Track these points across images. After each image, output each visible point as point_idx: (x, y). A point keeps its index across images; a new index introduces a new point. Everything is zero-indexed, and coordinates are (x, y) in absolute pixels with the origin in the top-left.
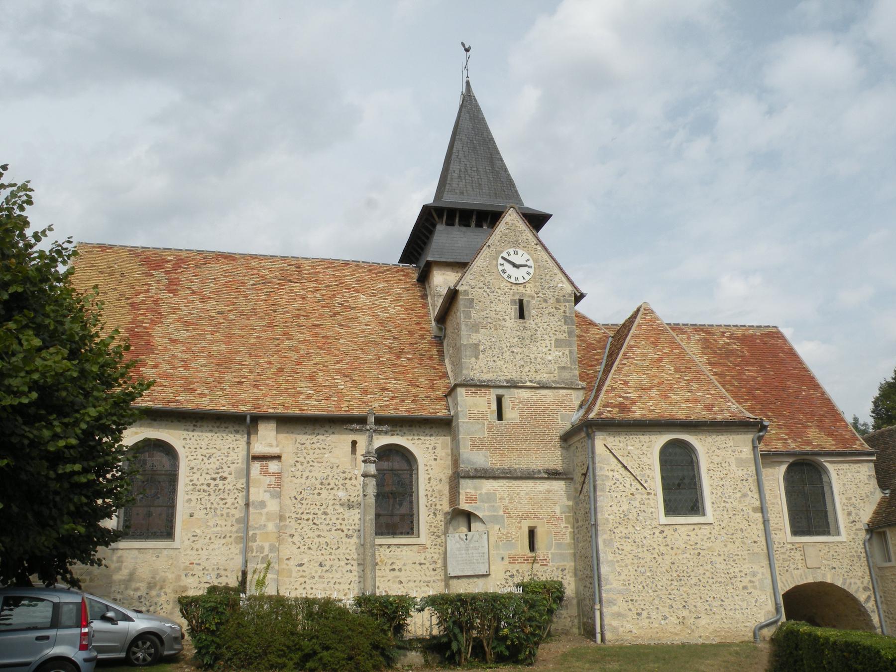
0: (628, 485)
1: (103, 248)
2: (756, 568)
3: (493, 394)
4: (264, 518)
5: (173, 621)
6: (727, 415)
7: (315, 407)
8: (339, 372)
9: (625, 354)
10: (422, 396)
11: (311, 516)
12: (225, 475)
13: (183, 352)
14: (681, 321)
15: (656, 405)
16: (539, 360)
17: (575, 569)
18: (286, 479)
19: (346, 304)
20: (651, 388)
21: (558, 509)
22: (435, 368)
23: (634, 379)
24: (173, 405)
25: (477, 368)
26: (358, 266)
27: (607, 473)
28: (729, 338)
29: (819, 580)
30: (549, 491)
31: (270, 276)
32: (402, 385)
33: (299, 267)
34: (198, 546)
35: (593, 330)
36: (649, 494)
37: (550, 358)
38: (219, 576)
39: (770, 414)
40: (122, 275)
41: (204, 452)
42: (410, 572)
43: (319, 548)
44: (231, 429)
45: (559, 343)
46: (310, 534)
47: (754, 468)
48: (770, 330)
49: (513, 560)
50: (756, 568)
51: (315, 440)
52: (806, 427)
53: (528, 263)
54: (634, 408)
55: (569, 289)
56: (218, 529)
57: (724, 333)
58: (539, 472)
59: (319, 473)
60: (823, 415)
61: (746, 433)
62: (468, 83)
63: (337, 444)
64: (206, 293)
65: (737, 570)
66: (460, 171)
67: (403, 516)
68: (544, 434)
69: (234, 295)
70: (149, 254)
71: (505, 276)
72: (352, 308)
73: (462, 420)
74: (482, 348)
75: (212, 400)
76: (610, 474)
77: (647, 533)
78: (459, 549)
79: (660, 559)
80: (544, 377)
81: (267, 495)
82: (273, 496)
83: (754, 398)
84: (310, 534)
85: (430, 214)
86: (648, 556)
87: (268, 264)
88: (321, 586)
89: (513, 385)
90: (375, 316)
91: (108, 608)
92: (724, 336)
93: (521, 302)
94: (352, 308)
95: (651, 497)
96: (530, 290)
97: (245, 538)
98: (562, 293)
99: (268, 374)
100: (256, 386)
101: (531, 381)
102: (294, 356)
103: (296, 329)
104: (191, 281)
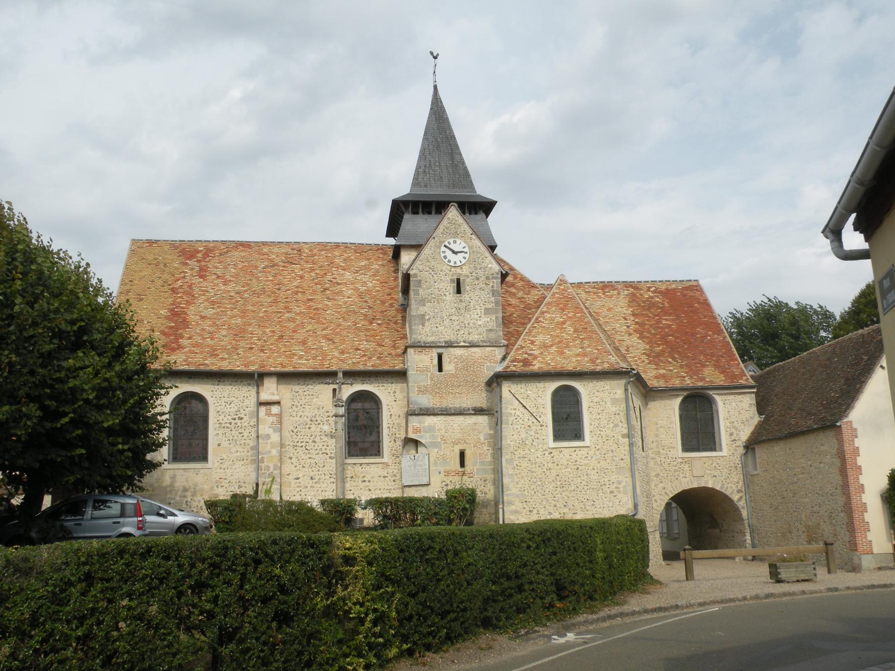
0: (526, 420)
1: (151, 242)
2: (621, 478)
3: (434, 353)
4: (269, 446)
5: (203, 517)
6: (606, 366)
7: (305, 365)
8: (325, 337)
9: (537, 319)
10: (386, 353)
11: (304, 444)
12: (242, 416)
13: (210, 326)
14: (613, 279)
15: (552, 359)
16: (471, 325)
17: (494, 480)
18: (286, 418)
19: (334, 281)
20: (552, 346)
21: (482, 438)
22: (398, 331)
23: (540, 339)
24: (202, 368)
25: (422, 333)
26: (346, 247)
27: (511, 411)
28: (653, 292)
29: (703, 485)
30: (475, 424)
31: (277, 260)
32: (371, 346)
33: (299, 251)
34: (225, 466)
35: (534, 292)
36: (542, 426)
37: (480, 323)
38: (240, 487)
39: (676, 356)
40: (165, 265)
41: (226, 400)
42: (371, 482)
43: (310, 466)
44: (245, 382)
45: (487, 311)
46: (304, 457)
47: (624, 405)
48: (691, 283)
49: (447, 474)
50: (621, 478)
51: (306, 389)
52: (704, 366)
53: (465, 250)
54: (535, 362)
55: (496, 268)
56: (239, 454)
57: (650, 288)
58: (469, 409)
59: (309, 412)
60: (722, 356)
61: (620, 379)
62: (435, 87)
63: (322, 393)
64: (228, 277)
65: (606, 480)
66: (425, 166)
67: (372, 442)
68: (473, 381)
69: (248, 277)
70: (186, 246)
71: (446, 261)
72: (338, 284)
73: (410, 373)
74: (427, 317)
75: (230, 363)
76: (513, 412)
77: (539, 454)
78: (410, 466)
79: (548, 473)
80: (474, 338)
81: (271, 430)
82: (275, 431)
83: (666, 343)
84: (304, 457)
85: (399, 205)
86: (539, 471)
87: (276, 250)
88: (312, 493)
89: (450, 345)
90: (356, 289)
91: (160, 508)
92: (649, 290)
93: (458, 281)
94: (338, 284)
95: (543, 428)
96: (465, 271)
97: (257, 462)
98: (491, 272)
99: (272, 340)
100: (262, 351)
101: (464, 342)
102: (292, 325)
103: (294, 303)
104: (216, 268)
